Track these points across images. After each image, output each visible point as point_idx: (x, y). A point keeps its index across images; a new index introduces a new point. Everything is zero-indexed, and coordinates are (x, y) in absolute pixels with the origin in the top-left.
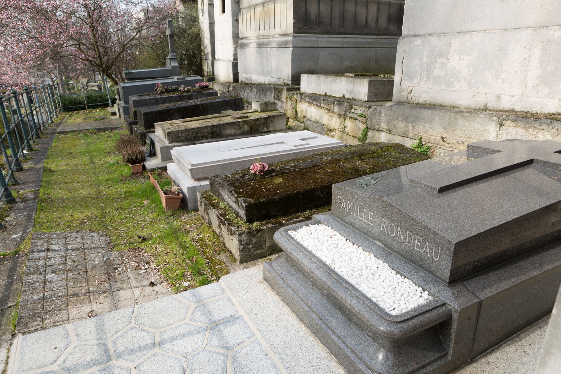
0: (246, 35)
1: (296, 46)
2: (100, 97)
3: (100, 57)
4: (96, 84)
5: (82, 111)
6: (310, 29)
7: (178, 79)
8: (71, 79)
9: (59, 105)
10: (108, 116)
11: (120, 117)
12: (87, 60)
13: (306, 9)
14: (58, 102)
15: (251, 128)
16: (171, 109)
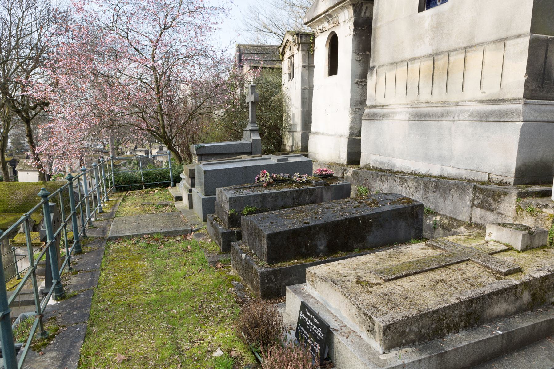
0: (381, 101)
1: (528, 119)
2: (160, 174)
3: (163, 127)
4: (144, 149)
5: (137, 192)
6: (548, 92)
7: (279, 160)
8: (120, 144)
9: (111, 183)
10: (171, 202)
11: (191, 206)
12: (149, 130)
13: (546, 58)
14: (111, 180)
15: (534, 296)
16: (314, 227)
